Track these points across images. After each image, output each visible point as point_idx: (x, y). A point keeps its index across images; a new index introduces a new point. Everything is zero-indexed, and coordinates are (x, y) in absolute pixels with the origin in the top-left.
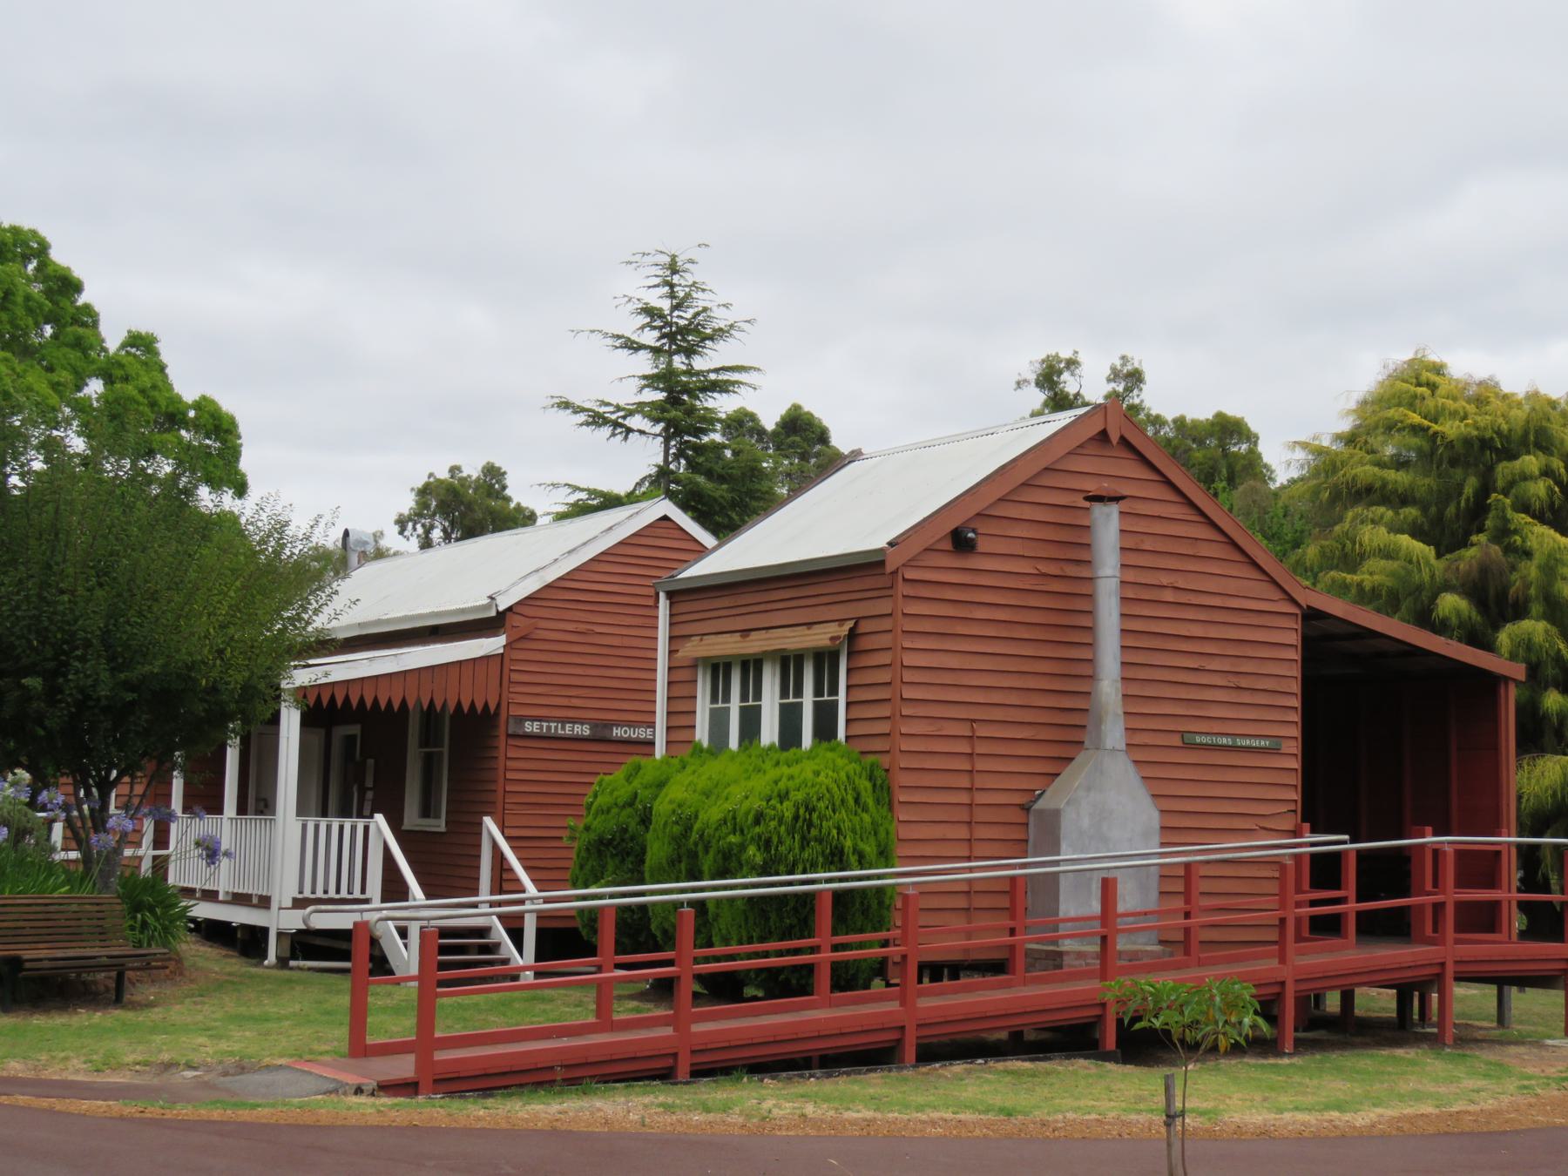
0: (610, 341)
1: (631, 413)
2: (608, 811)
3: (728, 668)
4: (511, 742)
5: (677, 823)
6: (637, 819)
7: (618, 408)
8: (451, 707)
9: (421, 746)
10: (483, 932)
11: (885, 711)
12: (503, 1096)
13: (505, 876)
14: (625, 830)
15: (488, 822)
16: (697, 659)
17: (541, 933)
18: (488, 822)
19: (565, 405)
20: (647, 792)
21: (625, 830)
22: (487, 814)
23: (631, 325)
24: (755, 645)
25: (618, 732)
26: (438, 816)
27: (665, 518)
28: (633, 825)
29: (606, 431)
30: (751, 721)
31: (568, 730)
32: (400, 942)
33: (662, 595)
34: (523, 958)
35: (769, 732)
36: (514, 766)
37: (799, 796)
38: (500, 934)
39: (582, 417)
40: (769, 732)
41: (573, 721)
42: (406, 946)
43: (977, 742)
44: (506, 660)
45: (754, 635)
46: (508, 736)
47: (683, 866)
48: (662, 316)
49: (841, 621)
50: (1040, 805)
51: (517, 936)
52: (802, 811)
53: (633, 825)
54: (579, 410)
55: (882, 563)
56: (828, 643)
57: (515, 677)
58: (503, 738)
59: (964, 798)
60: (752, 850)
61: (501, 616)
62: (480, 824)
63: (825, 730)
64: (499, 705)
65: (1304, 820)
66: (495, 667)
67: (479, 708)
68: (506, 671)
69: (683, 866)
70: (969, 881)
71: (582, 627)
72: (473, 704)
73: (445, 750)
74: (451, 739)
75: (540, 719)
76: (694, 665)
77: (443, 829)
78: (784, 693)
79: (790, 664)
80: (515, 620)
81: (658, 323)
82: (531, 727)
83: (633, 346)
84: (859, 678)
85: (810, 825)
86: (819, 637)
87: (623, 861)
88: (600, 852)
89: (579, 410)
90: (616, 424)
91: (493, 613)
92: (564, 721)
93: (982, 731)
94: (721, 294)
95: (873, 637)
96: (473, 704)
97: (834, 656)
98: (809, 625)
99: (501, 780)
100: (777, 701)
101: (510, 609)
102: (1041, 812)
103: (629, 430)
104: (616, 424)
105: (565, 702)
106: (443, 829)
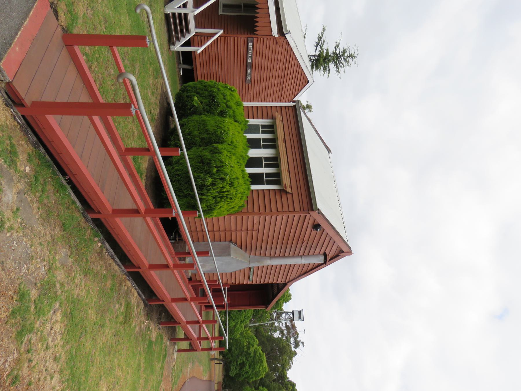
0: (338, 42)
1: (321, 48)
2: (225, 99)
3: (272, 132)
4: (246, 39)
5: (221, 133)
6: (222, 110)
7: (323, 45)
8: (256, 15)
9: (266, 174)
10: (188, 30)
11: (262, 210)
12: (40, 157)
13: (206, 37)
14: (218, 106)
15: (222, 31)
16: (275, 119)
17: (190, 53)
18: (222, 31)
19: (324, 30)
20: (231, 112)
21: (218, 106)
22: (224, 31)
23: (341, 48)
24: (281, 146)
25: (249, 70)
26: (223, 12)
27: (308, 82)
28: (219, 109)
29: (317, 41)
30: (254, 144)
31: (249, 56)
32: (181, 4)
33: (294, 104)
34: (178, 47)
35: (253, 153)
36: (239, 40)
37: (232, 191)
38: (188, 37)
39: (321, 35)
40: (253, 153)
41: (252, 57)
42: (180, 7)
43: (251, 232)
44: (270, 37)
45: (284, 144)
46: (248, 38)
47: (206, 136)
48: (343, 55)
49: (291, 186)
50: (232, 246)
51: (187, 44)
52: (226, 193)
53: (219, 109)
54: (322, 34)
55: (312, 210)
56: (284, 183)
57: (265, 40)
58: (247, 36)
59: (233, 228)
60: (210, 180)
61: (284, 35)
62: (221, 29)
63: (256, 179)
64: (257, 35)
65: (230, 285)
66: (269, 34)
67: (256, 28)
68: (267, 37)
69: (206, 136)
70: (205, 231)
71: (279, 59)
72: (257, 26)
73: (243, 14)
74: (246, 16)
75: (253, 47)
76: (273, 118)
77: (220, 13)
78: (266, 159)
79: (278, 175)
80: (282, 39)
81: (341, 54)
82: (250, 45)
83: (337, 47)
84: (272, 194)
85: (221, 198)
86: (286, 179)
87: (207, 105)
88: (210, 96)
89: (322, 34)
90: (318, 43)
91: (284, 33)
92: (252, 55)
93: (255, 233)
94: (349, 70)
95: (286, 198)
96: (257, 26)
97: (278, 182)
98: (289, 171)
99: (235, 36)
100: (260, 124)
101: (286, 38)
102: (229, 247)
103: (317, 46)
104: (318, 43)
105: (258, 55)
106: (220, 13)
